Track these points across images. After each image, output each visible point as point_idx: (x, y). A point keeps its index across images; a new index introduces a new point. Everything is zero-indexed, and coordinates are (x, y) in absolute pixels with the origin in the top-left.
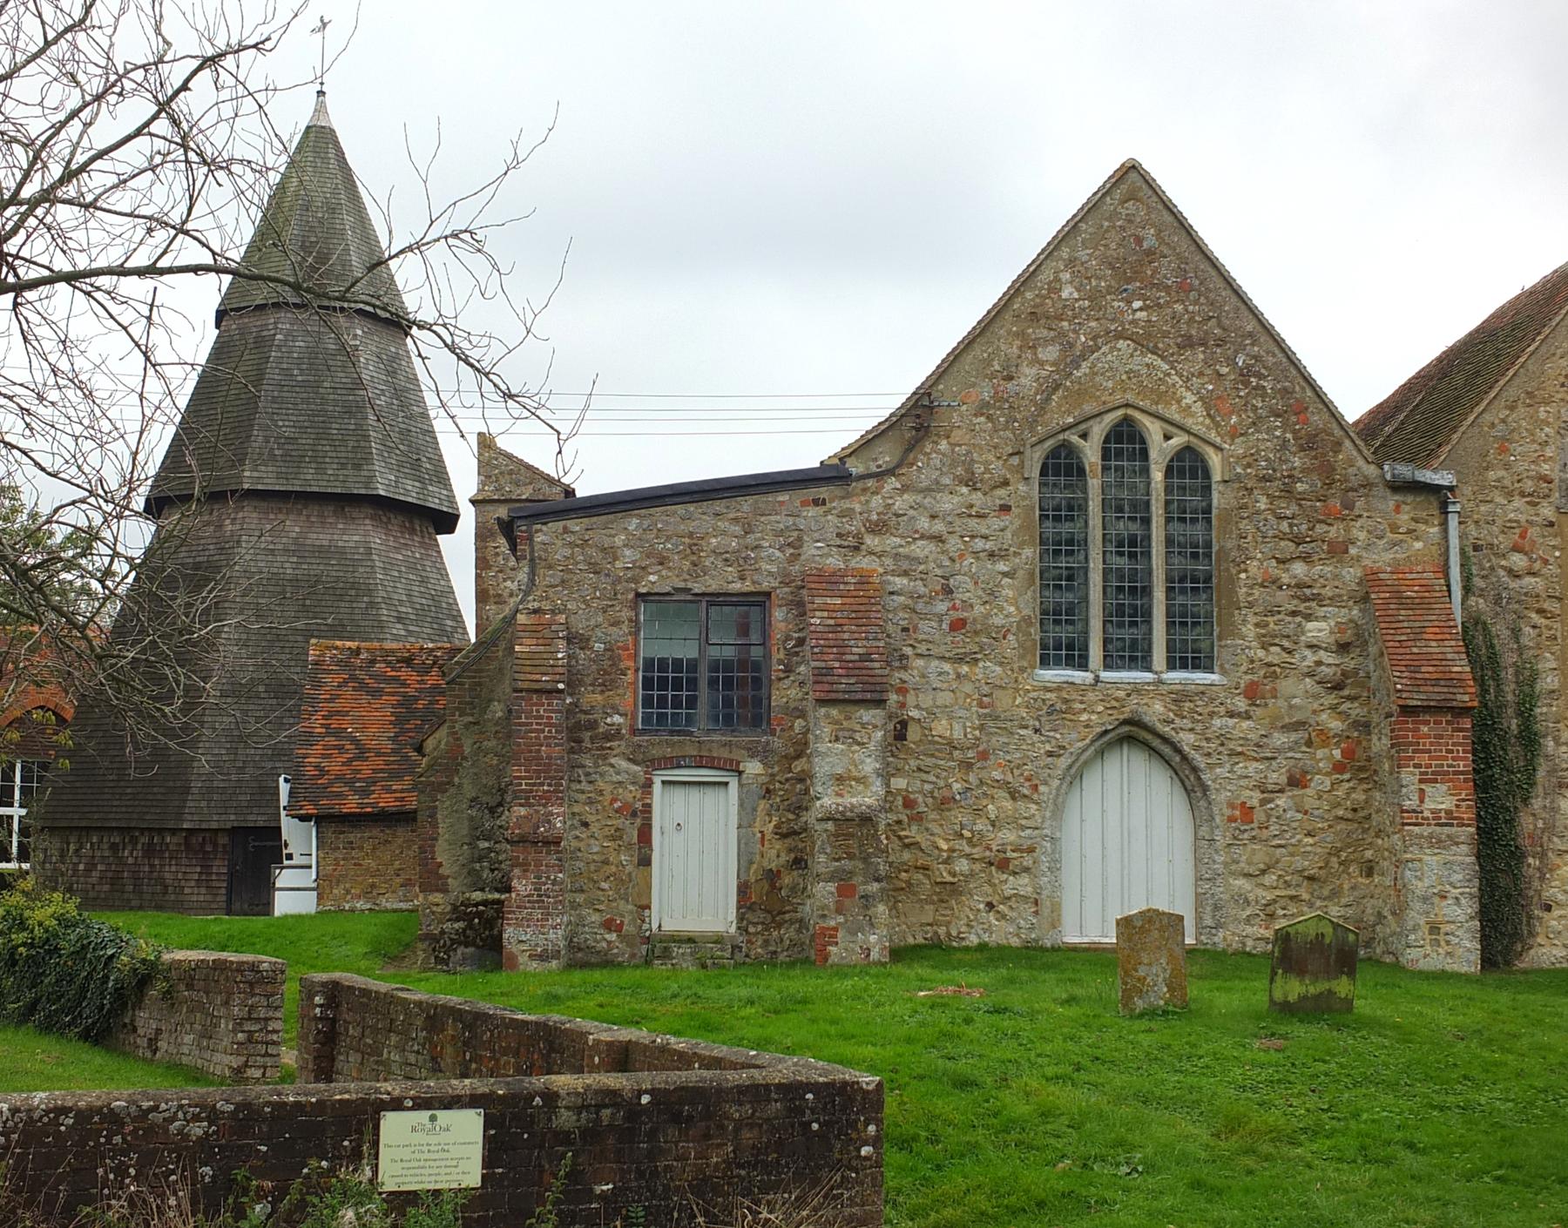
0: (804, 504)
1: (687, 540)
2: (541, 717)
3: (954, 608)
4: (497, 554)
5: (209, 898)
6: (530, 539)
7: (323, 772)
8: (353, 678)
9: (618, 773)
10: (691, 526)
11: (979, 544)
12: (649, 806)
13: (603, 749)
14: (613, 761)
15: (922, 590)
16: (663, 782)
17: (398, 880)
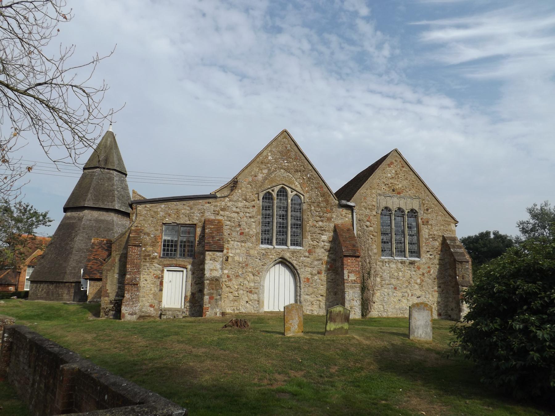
0: (206, 203)
8: (102, 247)
10: (178, 207)
11: (248, 215)
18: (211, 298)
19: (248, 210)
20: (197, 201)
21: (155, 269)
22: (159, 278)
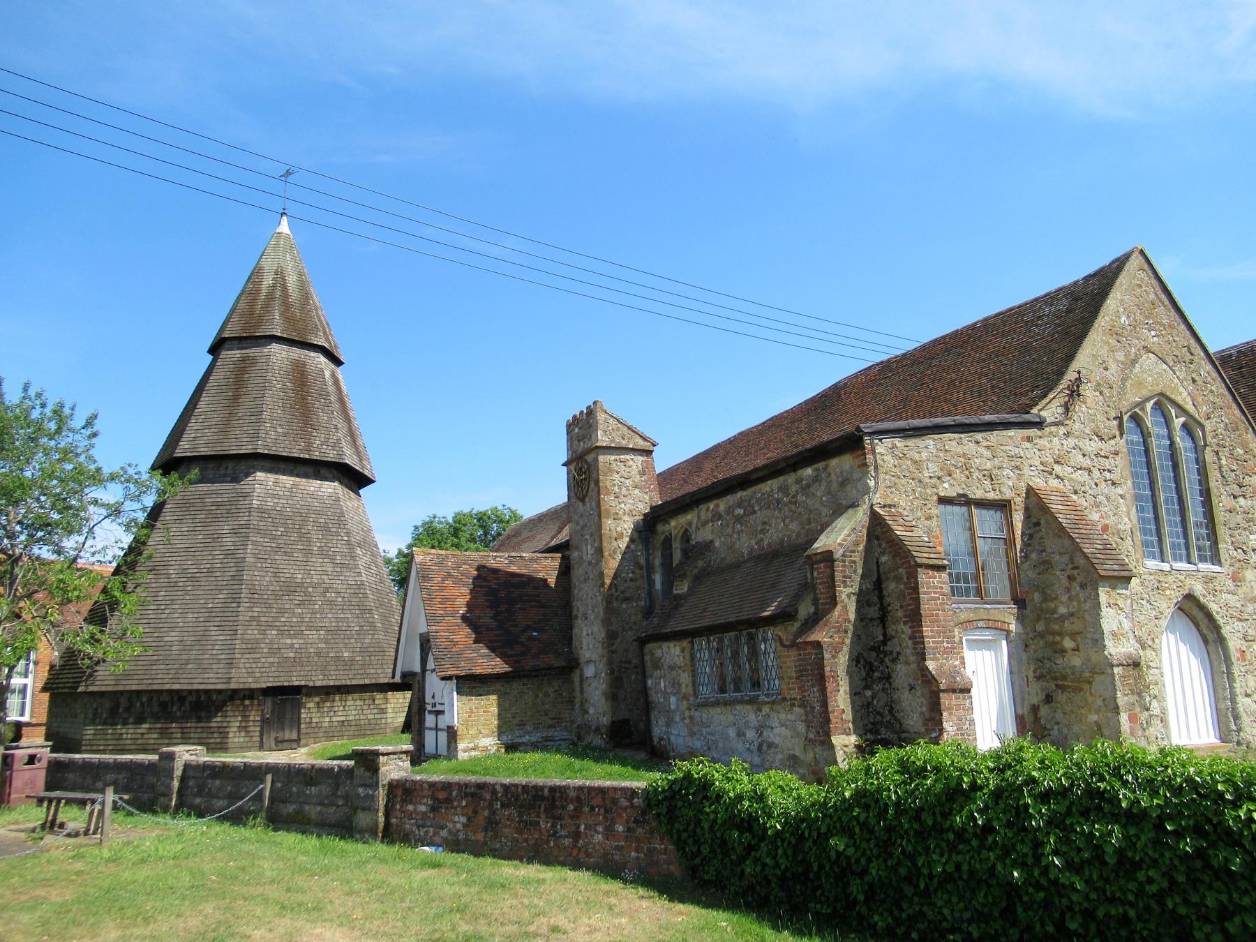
6: (873, 450)
8: (450, 575)
11: (1108, 475)
15: (1085, 504)
17: (516, 721)
18: (1133, 718)
19: (1106, 464)
20: (1004, 433)
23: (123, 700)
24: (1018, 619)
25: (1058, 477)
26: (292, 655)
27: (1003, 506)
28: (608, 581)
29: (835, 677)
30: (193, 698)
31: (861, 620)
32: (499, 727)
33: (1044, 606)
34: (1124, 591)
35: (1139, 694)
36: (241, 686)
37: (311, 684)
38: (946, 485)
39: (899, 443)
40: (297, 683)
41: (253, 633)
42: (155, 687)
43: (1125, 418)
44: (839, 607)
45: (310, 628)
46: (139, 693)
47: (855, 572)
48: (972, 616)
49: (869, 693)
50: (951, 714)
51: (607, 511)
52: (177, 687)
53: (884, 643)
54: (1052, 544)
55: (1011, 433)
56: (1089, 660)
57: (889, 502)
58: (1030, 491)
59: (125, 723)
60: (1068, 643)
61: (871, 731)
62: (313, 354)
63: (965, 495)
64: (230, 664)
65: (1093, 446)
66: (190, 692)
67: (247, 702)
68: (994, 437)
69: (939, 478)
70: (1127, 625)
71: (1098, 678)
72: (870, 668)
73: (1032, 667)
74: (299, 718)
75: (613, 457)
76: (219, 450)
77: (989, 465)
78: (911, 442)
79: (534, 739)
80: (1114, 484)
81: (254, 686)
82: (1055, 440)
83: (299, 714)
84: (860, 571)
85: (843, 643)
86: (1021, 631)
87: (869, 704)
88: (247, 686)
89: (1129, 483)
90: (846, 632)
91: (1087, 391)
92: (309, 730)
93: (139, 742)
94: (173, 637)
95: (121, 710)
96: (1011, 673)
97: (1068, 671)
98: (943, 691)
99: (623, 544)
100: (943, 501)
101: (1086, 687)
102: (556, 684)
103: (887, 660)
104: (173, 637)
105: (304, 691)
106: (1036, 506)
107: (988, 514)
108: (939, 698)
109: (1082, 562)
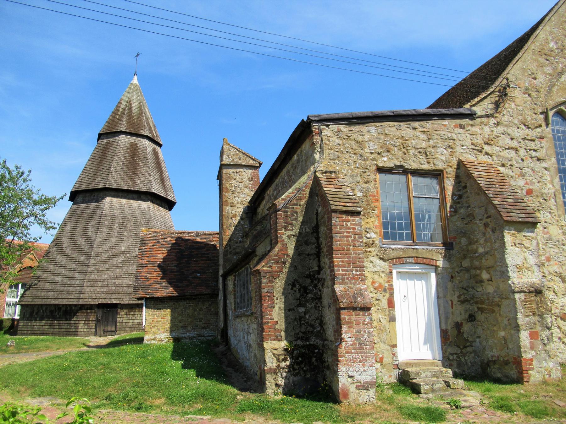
0: (456, 126)
1: (400, 141)
2: (349, 228)
3: (527, 183)
4: (232, 186)
5: (88, 330)
6: (320, 134)
7: (148, 279)
8: (158, 243)
9: (375, 266)
10: (403, 133)
11: (534, 154)
12: (392, 285)
13: (366, 252)
14: (371, 259)
15: (512, 174)
16: (398, 273)
17: (181, 325)
18: (534, 335)
19: (532, 145)
20: (439, 122)
21: (374, 269)
22: (385, 290)
23: (36, 309)
24: (445, 257)
25: (487, 154)
26: (114, 288)
27: (437, 175)
28: (225, 243)
29: (271, 298)
30: (64, 308)
31: (299, 255)
32: (171, 328)
33: (470, 248)
34: (530, 234)
35: (541, 316)
36: (85, 303)
37: (122, 303)
38: (385, 159)
39: (344, 128)
40: (115, 302)
41: (94, 275)
42: (48, 303)
43: (551, 114)
44: (279, 245)
45: (125, 274)
46: (42, 305)
47: (296, 219)
48: (401, 254)
49: (302, 310)
50: (351, 327)
51: (227, 202)
52: (57, 303)
53: (319, 272)
54: (474, 200)
55: (445, 122)
56: (498, 287)
57: (331, 169)
58: (460, 164)
59: (36, 320)
60: (485, 276)
61: (302, 339)
62: (142, 140)
63: (401, 167)
64: (81, 292)
65: (523, 132)
66: (63, 305)
67: (89, 311)
68: (429, 125)
69: (379, 154)
70: (532, 260)
71: (505, 302)
72: (305, 290)
73: (457, 294)
74: (116, 320)
75: (232, 170)
76: (90, 187)
77: (424, 145)
78: (355, 128)
79: (191, 335)
80: (539, 160)
81: (92, 303)
82: (486, 128)
83: (116, 318)
84: (301, 219)
85: (281, 271)
86: (447, 265)
87: (301, 318)
88: (88, 303)
89: (554, 160)
90: (284, 263)
91: (516, 94)
92: (121, 327)
93: (41, 329)
94: (59, 278)
95: (34, 314)
96: (438, 297)
97: (485, 297)
98: (344, 308)
99: (236, 221)
100: (381, 170)
101: (496, 309)
102: (207, 304)
103: (320, 285)
104: (59, 278)
105: (119, 306)
106: (463, 174)
107: (426, 181)
108: (339, 314)
109: (492, 211)
